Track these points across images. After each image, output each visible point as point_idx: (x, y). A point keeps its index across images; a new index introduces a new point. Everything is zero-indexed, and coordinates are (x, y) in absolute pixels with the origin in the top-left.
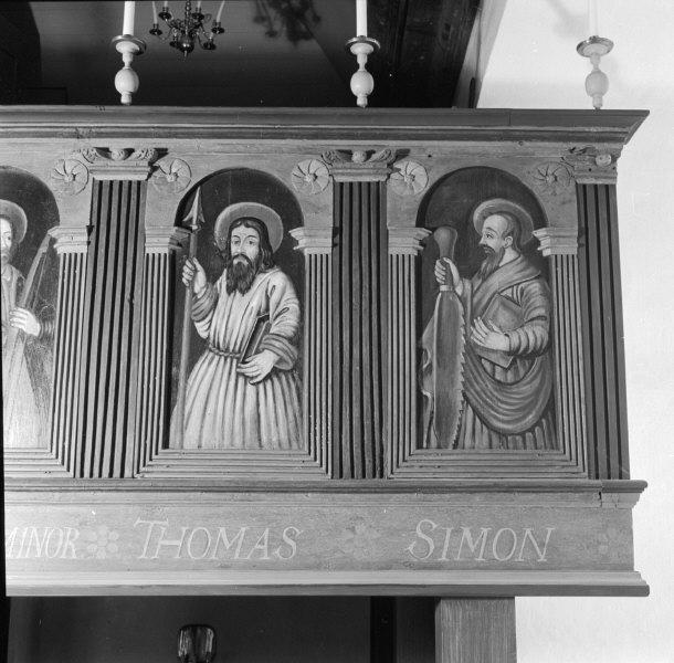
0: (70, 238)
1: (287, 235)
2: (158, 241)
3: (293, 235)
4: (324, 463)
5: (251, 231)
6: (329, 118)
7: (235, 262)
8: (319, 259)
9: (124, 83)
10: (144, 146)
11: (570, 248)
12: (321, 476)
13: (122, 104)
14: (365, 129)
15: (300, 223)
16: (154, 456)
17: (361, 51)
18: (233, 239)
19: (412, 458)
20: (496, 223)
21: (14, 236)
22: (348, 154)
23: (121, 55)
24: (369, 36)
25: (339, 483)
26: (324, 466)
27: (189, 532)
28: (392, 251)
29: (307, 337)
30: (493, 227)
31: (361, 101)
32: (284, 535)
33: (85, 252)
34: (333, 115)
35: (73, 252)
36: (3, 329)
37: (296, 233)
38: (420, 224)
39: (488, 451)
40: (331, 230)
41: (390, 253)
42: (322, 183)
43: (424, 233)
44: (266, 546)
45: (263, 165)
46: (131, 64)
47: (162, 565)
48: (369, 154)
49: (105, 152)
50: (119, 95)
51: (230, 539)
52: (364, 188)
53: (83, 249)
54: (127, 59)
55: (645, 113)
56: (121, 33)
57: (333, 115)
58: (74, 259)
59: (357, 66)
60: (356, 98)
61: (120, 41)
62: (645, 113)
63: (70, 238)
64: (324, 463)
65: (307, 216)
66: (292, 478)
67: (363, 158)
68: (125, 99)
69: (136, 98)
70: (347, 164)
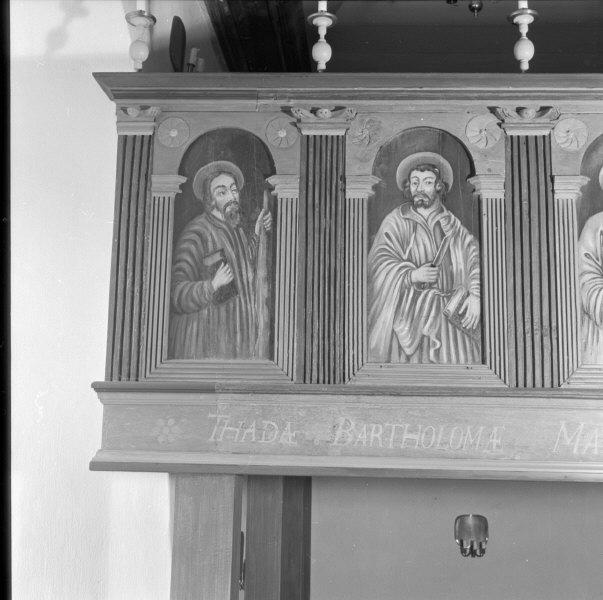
0: (287, 188)
5: (427, 174)
6: (503, 84)
7: (416, 199)
9: (525, 51)
15: (273, 172)
16: (351, 375)
17: (525, 21)
19: (158, 371)
28: (350, 194)
31: (525, 66)
33: (503, 198)
35: (494, 197)
36: (600, 263)
38: (181, 172)
41: (347, 198)
43: (183, 180)
48: (144, 108)
50: (519, 63)
51: (473, 437)
52: (522, 141)
55: (97, 76)
56: (317, 11)
57: (586, 80)
59: (318, 37)
62: (97, 76)
63: (287, 188)
68: (525, 66)
69: (537, 65)
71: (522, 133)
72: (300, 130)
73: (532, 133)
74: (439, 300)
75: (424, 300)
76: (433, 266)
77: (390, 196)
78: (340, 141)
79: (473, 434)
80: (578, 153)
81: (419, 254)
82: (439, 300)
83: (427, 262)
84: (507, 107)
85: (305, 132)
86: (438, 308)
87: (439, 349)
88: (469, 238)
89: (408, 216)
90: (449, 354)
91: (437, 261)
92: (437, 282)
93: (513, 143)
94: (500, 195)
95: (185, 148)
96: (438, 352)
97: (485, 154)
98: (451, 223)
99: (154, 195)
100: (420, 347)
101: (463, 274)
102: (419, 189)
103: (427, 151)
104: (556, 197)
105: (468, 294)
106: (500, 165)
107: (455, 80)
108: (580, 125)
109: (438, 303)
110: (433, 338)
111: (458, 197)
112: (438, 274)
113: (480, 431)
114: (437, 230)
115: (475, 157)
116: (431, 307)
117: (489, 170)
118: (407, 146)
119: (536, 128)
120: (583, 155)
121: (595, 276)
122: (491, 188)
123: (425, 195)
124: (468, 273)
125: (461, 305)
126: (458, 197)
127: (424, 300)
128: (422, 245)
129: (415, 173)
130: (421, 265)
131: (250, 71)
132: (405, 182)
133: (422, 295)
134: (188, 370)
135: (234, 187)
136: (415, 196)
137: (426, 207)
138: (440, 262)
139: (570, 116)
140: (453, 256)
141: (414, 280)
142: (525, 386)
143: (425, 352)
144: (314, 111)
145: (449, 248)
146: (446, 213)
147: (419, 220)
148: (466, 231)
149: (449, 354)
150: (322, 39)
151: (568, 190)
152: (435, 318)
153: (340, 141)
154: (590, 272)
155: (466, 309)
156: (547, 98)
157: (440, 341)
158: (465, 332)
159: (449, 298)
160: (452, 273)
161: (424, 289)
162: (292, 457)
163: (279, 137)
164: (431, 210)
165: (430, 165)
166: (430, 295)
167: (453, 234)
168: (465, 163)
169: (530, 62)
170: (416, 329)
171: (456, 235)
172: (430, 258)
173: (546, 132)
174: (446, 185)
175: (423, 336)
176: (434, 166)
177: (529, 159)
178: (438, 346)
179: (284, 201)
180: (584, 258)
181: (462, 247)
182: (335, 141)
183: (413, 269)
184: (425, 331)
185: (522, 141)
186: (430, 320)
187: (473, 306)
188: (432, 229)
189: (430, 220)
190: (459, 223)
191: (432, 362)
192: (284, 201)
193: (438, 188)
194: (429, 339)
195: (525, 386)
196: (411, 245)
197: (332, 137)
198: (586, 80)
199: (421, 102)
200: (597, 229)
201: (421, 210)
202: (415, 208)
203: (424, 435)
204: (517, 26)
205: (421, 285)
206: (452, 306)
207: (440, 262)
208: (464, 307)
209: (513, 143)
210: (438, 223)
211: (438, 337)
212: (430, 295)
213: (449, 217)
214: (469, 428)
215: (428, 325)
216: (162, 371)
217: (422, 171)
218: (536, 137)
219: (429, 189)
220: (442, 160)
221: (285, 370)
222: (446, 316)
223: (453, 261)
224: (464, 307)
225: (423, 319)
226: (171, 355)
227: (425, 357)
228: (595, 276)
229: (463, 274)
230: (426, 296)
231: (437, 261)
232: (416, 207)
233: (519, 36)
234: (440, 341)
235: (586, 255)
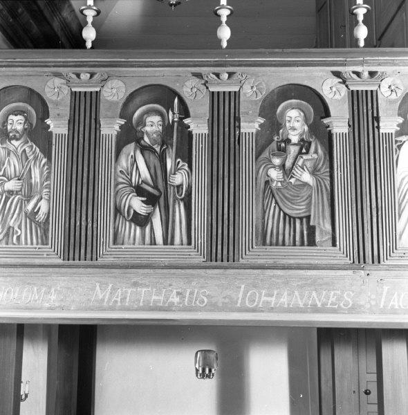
4: (59, 253)
5: (19, 117)
7: (11, 134)
9: (362, 32)
11: (64, 130)
12: (200, 260)
14: (195, 61)
16: (244, 256)
20: (293, 114)
21: (306, 120)
24: (364, 4)
25: (209, 263)
26: (199, 252)
30: (295, 121)
31: (89, 45)
35: (60, 133)
37: (186, 121)
38: (121, 117)
39: (25, 246)
42: (66, 92)
45: (34, 84)
47: (51, 309)
48: (92, 75)
49: (358, 74)
50: (84, 41)
56: (355, 4)
57: (324, 53)
58: (60, 136)
61: (218, 9)
63: (58, 126)
64: (59, 253)
65: (191, 114)
66: (336, 262)
68: (89, 45)
71: (360, 88)
72: (207, 88)
73: (227, 89)
74: (22, 202)
75: (12, 203)
76: (19, 179)
78: (237, 95)
80: (118, 103)
81: (11, 171)
82: (22, 202)
83: (15, 176)
84: (347, 70)
85: (211, 89)
86: (21, 208)
87: (20, 235)
88: (44, 160)
89: (4, 146)
90: (26, 239)
91: (22, 176)
92: (21, 190)
93: (74, 94)
94: (346, 130)
96: (18, 238)
97: (57, 104)
98: (32, 150)
100: (7, 235)
101: (39, 185)
102: (13, 128)
103: (20, 102)
104: (381, 131)
105: (41, 198)
108: (121, 84)
109: (22, 204)
110: (16, 228)
111: (319, 131)
112: (22, 185)
113: (43, 291)
114: (24, 155)
115: (50, 106)
116: (16, 207)
117: (58, 115)
118: (7, 99)
119: (90, 87)
120: (121, 105)
121: (125, 185)
122: (58, 126)
123: (18, 132)
124: (42, 184)
125: (36, 205)
126: (38, 135)
127: (12, 203)
128: (13, 165)
129: (11, 117)
130: (11, 179)
132: (4, 123)
133: (11, 199)
135: (160, 123)
136: (10, 132)
137: (17, 140)
138: (25, 177)
139: (392, 77)
140: (33, 173)
141: (6, 189)
143: (10, 238)
144: (218, 75)
145: (30, 168)
146: (30, 144)
147: (12, 148)
148: (42, 156)
149: (26, 239)
151: (390, 124)
152: (19, 215)
153: (237, 95)
154: (125, 183)
155: (39, 208)
157: (21, 230)
158: (38, 224)
159: (28, 201)
160: (31, 184)
161: (12, 195)
162: (183, 313)
163: (189, 89)
164: (19, 142)
165: (22, 111)
166: (16, 199)
167: (34, 157)
168: (322, 108)
169: (365, 40)
170: (5, 222)
171: (36, 158)
172: (18, 174)
173: (98, 89)
174: (31, 125)
175: (10, 227)
176: (24, 112)
177: (363, 106)
178: (19, 234)
179: (244, 134)
180: (119, 174)
181: (39, 166)
182: (82, 98)
183: (6, 181)
184: (11, 224)
186: (15, 216)
187: (44, 206)
188: (20, 155)
189: (19, 148)
190: (38, 150)
191: (14, 244)
192: (244, 134)
193: (26, 127)
194: (14, 228)
196: (5, 166)
197: (224, 92)
198: (296, 53)
199: (17, 69)
200: (129, 154)
201: (14, 142)
202: (10, 141)
203: (6, 293)
204: (356, 15)
205: (11, 193)
206: (30, 207)
207: (25, 177)
208: (37, 207)
209: (74, 94)
210: (24, 151)
211: (20, 228)
212: (16, 199)
213: (32, 147)
214: (35, 289)
215: (13, 220)
216: (253, 254)
217: (16, 115)
219: (20, 128)
220: (30, 108)
221: (342, 250)
222: (26, 214)
223: (33, 176)
224: (37, 207)
225: (10, 216)
227: (10, 240)
228: (125, 185)
229: (39, 185)
230: (14, 199)
231: (22, 176)
232: (10, 140)
233: (357, 22)
234: (21, 230)
235: (120, 171)
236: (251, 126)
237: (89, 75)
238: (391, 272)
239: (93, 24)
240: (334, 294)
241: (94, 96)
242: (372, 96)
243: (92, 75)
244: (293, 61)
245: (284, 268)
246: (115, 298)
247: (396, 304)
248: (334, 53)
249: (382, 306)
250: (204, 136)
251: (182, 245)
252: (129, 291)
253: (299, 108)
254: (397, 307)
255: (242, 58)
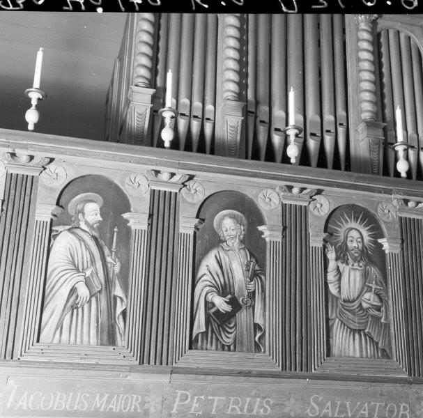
1: (376, 243)
2: (186, 225)
3: (124, 217)
8: (137, 233)
9: (32, 117)
10: (40, 157)
13: (28, 130)
16: (27, 350)
17: (34, 96)
18: (349, 239)
22: (290, 188)
23: (30, 99)
26: (135, 356)
27: (123, 396)
28: (181, 231)
29: (131, 276)
31: (31, 127)
32: (311, 400)
33: (280, 240)
34: (78, 142)
40: (148, 215)
44: (231, 407)
45: (249, 193)
46: (36, 106)
49: (157, 172)
50: (27, 124)
53: (280, 240)
54: (34, 102)
56: (32, 87)
58: (392, 254)
59: (31, 105)
60: (290, 158)
63: (137, 221)
67: (169, 177)
68: (31, 127)
69: (39, 128)
70: (289, 194)
77: (63, 218)
79: (100, 400)
84: (23, 155)
95: (200, 203)
99: (36, 218)
106: (145, 207)
107: (226, 161)
122: (270, 233)
131: (135, 145)
134: (193, 358)
142: (5, 358)
150: (33, 107)
156: (292, 181)
169: (35, 124)
185: (25, 177)
195: (5, 358)
209: (284, 206)
218: (165, 192)
226: (190, 348)
236: (186, 225)
237: (49, 160)
238: (23, 369)
239: (37, 108)
240: (198, 399)
241: (173, 196)
242: (304, 211)
243: (32, 158)
244: (315, 180)
245: (248, 374)
246: (20, 403)
247: (25, 404)
248: (103, 146)
249: (8, 406)
250: (137, 233)
251: (362, 357)
252: (378, 404)
253: (232, 217)
254: (25, 408)
255: (236, 167)
